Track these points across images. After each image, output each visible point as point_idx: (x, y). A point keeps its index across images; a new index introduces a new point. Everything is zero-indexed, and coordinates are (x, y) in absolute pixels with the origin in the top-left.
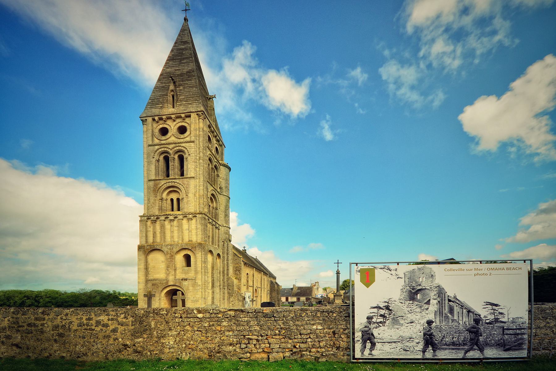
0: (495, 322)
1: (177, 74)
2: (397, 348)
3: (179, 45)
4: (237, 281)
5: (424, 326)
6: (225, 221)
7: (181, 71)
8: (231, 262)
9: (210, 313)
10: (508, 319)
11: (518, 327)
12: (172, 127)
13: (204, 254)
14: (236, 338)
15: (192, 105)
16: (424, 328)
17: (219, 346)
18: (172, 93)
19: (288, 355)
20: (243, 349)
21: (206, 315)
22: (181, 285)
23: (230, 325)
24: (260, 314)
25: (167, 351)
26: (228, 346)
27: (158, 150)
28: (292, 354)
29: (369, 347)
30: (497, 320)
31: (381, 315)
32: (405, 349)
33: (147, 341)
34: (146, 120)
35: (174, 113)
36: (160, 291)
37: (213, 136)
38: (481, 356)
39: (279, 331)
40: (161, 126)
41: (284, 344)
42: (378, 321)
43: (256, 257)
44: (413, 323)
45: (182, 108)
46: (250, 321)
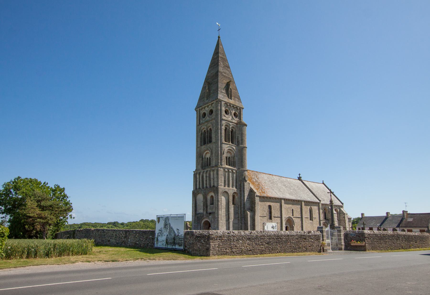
43: (323, 181)
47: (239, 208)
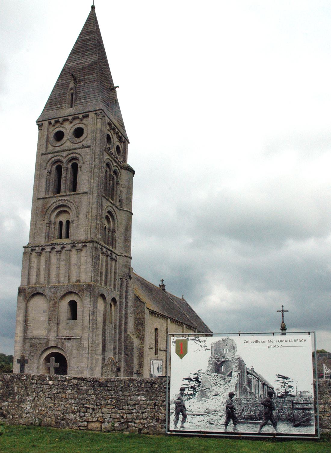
0: (286, 395)
1: (79, 69)
2: (204, 420)
3: (84, 36)
4: (139, 341)
5: (227, 399)
6: (125, 247)
7: (83, 64)
8: (132, 310)
9: (58, 380)
10: (297, 392)
11: (305, 402)
12: (68, 130)
13: (92, 301)
14: (77, 407)
15: (90, 103)
16: (226, 401)
17: (63, 413)
18: (72, 91)
19: (117, 426)
20: (81, 417)
21: (55, 383)
22: (64, 347)
23: (73, 393)
24: (97, 383)
25: (24, 415)
26: (70, 413)
27: (51, 159)
28: (120, 425)
29: (181, 420)
30: (287, 394)
31: (192, 387)
32: (210, 422)
33: (11, 405)
34: (42, 124)
35: (71, 114)
36: (39, 355)
37: (114, 134)
38: (274, 431)
39: (111, 401)
40: (57, 130)
41: (114, 414)
42: (190, 393)
43: (183, 296)
44: (217, 396)
45: (81, 107)
46: (89, 390)
47: (118, 331)
